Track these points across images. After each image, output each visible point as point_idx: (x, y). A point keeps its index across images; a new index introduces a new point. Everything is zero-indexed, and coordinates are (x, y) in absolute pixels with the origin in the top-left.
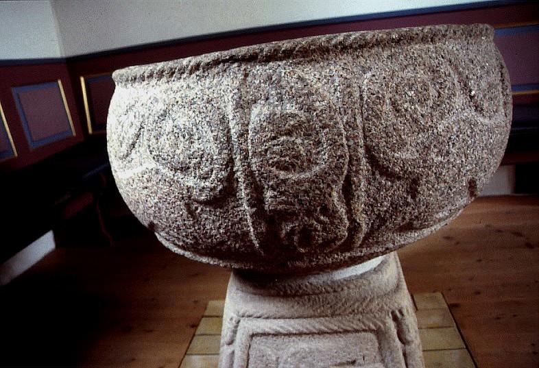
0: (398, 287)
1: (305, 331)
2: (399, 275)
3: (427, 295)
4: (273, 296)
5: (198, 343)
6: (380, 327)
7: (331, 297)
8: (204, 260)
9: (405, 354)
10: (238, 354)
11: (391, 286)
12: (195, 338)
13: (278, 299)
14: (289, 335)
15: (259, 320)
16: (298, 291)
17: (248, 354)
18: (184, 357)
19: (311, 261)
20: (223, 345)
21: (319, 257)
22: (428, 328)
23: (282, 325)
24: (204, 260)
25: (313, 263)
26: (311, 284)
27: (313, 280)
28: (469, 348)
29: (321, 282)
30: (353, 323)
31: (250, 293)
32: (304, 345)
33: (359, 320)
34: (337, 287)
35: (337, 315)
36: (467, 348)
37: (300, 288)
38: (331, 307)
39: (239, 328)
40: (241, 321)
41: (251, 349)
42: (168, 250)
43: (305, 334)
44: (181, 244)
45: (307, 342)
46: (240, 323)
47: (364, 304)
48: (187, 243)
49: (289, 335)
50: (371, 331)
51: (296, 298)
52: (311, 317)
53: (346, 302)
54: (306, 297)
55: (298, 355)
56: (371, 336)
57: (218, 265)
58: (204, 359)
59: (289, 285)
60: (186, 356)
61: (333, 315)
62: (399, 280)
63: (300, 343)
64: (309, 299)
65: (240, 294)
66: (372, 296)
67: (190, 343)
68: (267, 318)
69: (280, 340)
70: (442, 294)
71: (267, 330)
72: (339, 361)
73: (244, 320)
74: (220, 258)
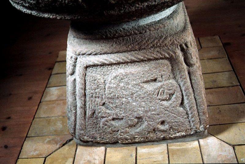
0: (184, 29)
1: (122, 61)
2: (186, 20)
3: (209, 38)
4: (98, 39)
5: (53, 80)
6: (172, 56)
7: (138, 37)
8: (46, 16)
9: (189, 73)
10: (78, 80)
11: (180, 28)
12: (52, 76)
13: (102, 41)
14: (111, 64)
15: (90, 56)
16: (115, 35)
17: (85, 80)
18: (45, 89)
19: (120, 10)
20: (68, 76)
21: (126, 7)
22: (208, 59)
23: (107, 58)
24: (46, 16)
25: (122, 12)
26: (124, 29)
27: (125, 26)
28: (235, 70)
29: (131, 27)
30: (153, 54)
31: (83, 39)
32: (121, 70)
33: (158, 51)
34: (142, 30)
35: (143, 49)
36: (234, 70)
37: (116, 32)
38: (138, 44)
39: (77, 63)
40: (78, 58)
41: (87, 76)
42: (20, 12)
43: (122, 63)
44: (27, 5)
45: (124, 69)
46: (78, 60)
47: (161, 41)
48: (31, 3)
49: (111, 64)
50: (166, 58)
51: (115, 40)
52: (125, 52)
53: (148, 40)
54: (121, 38)
55: (118, 78)
56: (166, 62)
57: (56, 18)
58: (58, 89)
59: (109, 31)
60: (46, 88)
61: (140, 49)
62: (185, 24)
63: (119, 70)
64: (123, 40)
65: (76, 40)
66: (166, 35)
67: (49, 80)
68: (96, 54)
69: (105, 69)
70: (219, 36)
71: (96, 62)
72: (145, 79)
73: (80, 57)
74: (57, 13)
